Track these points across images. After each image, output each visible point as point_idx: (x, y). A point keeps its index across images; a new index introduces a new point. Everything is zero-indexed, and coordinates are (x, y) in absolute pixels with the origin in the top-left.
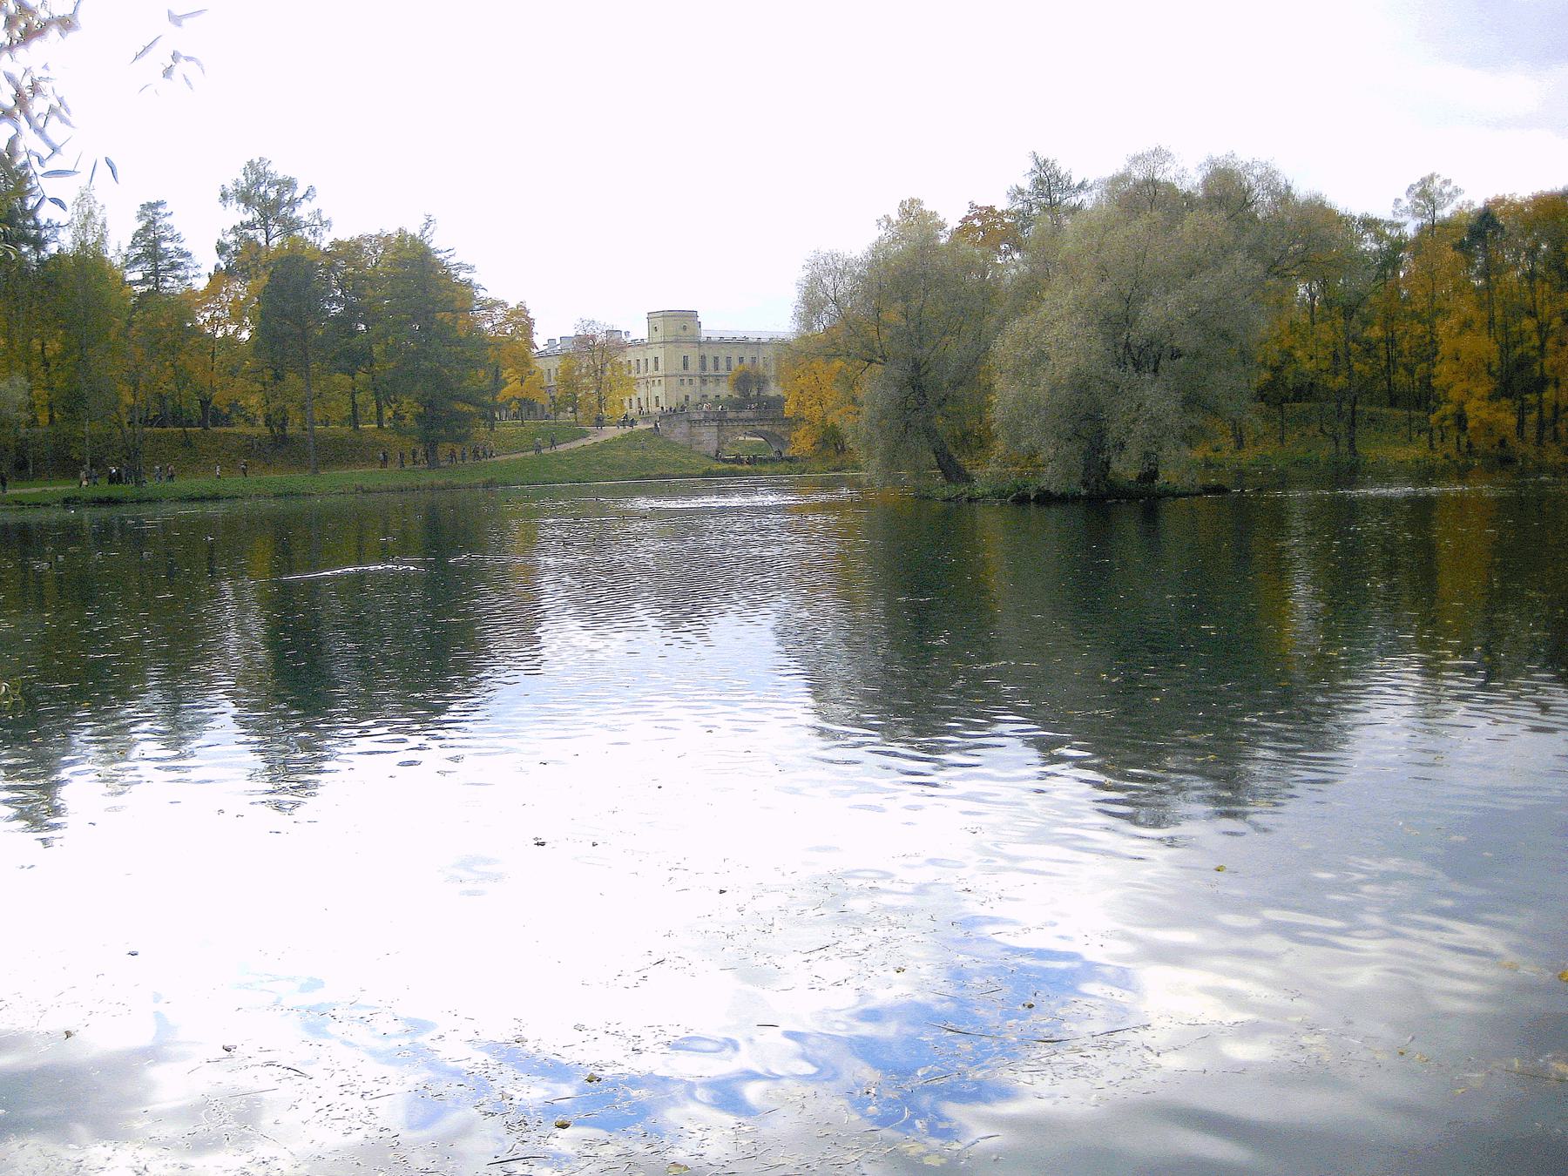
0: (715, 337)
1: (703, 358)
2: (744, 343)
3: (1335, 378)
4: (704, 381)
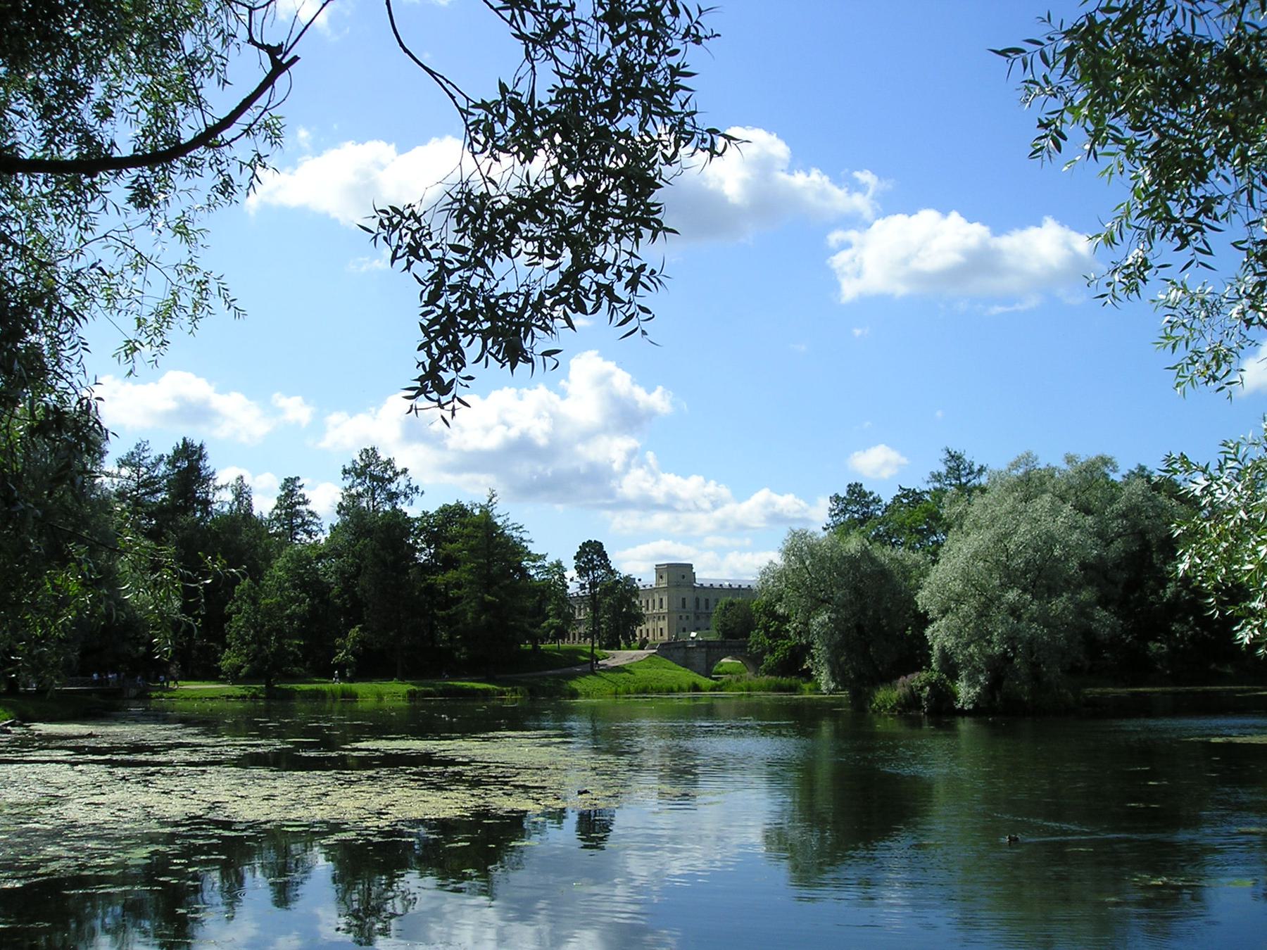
0: (707, 585)
1: (697, 600)
2: (731, 590)
3: (954, 635)
4: (698, 618)
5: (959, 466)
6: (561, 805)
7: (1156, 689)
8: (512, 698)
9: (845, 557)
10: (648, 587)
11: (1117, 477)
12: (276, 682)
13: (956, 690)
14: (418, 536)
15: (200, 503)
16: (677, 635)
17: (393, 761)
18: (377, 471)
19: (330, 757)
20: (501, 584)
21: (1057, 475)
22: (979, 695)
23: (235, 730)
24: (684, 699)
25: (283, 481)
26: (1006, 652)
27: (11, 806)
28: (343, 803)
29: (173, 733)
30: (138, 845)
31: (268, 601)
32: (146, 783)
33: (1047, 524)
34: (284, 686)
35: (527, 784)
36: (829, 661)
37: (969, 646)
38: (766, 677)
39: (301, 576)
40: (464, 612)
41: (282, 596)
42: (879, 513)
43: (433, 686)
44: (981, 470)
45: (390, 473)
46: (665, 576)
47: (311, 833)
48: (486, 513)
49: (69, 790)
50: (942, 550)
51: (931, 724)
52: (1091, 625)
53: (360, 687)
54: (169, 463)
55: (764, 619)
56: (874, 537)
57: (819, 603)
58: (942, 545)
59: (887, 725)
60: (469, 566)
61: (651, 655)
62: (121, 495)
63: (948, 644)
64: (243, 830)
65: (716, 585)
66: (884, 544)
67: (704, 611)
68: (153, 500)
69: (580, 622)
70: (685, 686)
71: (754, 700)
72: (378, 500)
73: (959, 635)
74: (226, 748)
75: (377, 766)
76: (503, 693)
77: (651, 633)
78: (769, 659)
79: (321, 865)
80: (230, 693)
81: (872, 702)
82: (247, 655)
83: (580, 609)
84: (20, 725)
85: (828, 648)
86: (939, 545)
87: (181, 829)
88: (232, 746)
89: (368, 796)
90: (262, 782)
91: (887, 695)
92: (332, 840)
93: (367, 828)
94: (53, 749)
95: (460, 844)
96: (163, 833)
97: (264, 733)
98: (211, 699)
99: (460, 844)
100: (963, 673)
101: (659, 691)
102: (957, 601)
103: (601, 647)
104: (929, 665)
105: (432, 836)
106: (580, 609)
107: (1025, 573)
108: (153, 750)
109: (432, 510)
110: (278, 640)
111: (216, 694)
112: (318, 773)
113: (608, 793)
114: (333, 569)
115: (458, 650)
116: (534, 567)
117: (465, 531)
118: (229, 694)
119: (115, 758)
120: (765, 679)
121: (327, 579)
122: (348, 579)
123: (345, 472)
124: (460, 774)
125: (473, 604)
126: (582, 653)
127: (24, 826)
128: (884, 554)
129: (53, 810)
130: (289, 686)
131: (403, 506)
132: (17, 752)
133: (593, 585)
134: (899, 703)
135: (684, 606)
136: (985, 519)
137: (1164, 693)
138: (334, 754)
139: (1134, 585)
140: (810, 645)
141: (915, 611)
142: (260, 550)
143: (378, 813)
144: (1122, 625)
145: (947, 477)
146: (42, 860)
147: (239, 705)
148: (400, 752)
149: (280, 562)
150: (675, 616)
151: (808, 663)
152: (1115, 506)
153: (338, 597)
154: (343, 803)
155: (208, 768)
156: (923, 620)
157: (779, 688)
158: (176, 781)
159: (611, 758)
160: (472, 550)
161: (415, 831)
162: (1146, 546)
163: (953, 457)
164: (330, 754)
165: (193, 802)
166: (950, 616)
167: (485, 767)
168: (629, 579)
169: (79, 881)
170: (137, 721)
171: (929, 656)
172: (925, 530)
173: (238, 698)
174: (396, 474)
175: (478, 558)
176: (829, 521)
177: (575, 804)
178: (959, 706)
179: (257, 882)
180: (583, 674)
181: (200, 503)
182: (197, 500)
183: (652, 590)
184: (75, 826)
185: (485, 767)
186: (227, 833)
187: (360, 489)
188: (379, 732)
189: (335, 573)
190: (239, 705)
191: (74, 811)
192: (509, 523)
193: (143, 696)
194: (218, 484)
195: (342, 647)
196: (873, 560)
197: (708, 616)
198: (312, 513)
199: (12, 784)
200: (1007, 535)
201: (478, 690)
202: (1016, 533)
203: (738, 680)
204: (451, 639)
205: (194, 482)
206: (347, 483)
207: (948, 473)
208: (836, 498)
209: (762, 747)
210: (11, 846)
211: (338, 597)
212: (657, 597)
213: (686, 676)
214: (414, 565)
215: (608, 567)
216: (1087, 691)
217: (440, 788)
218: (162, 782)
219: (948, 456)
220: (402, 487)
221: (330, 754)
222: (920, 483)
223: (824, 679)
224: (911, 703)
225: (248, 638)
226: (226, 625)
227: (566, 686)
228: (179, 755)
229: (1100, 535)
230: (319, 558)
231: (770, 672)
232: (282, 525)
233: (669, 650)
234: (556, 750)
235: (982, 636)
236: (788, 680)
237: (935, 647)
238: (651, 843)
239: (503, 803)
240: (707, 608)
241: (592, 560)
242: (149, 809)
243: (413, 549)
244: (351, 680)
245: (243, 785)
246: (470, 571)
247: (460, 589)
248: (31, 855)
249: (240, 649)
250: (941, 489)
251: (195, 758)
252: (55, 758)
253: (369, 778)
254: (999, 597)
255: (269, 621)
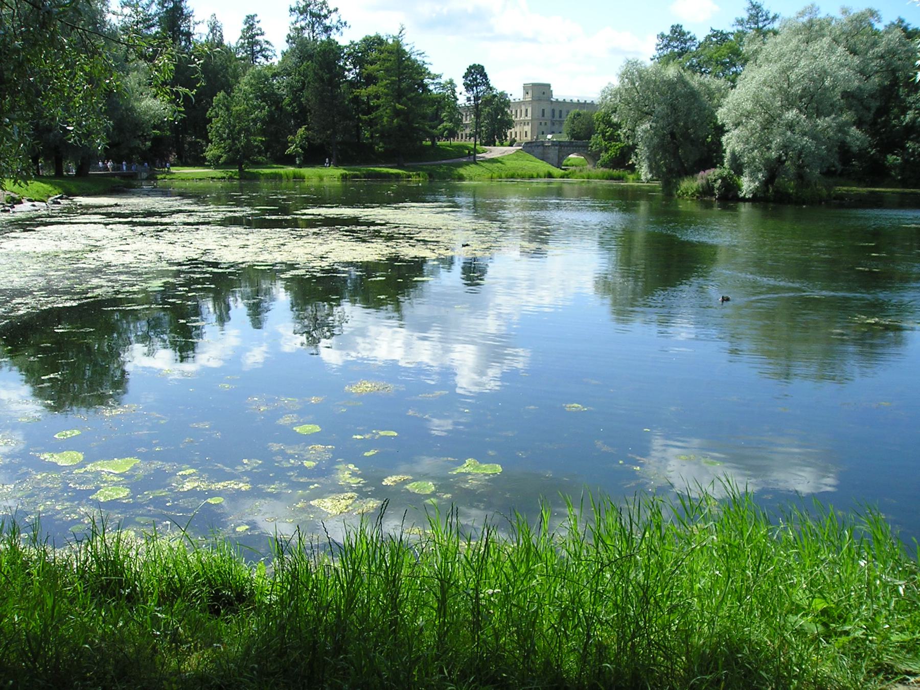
0: (561, 100)
1: (553, 111)
2: (579, 104)
3: (743, 142)
4: (553, 124)
5: (758, 14)
6: (449, 253)
7: (889, 190)
8: (417, 180)
9: (665, 81)
10: (517, 100)
11: (880, 27)
12: (246, 167)
13: (740, 182)
14: (347, 59)
15: (184, 34)
16: (537, 136)
17: (331, 222)
18: (315, 10)
19: (286, 219)
20: (409, 96)
21: (833, 23)
22: (757, 188)
23: (218, 201)
24: (541, 183)
25: (245, 18)
26: (780, 156)
27: (65, 252)
28: (296, 251)
29: (175, 203)
30: (155, 278)
31: (238, 108)
32: (158, 237)
33: (825, 62)
34: (252, 170)
35: (426, 239)
36: (648, 158)
37: (753, 151)
38: (601, 169)
39: (260, 89)
40: (381, 117)
41: (247, 105)
42: (694, 48)
43: (359, 171)
44: (775, 18)
45: (325, 12)
46: (530, 92)
47: (272, 272)
48: (397, 43)
49: (104, 242)
50: (739, 77)
51: (719, 207)
52: (846, 138)
53: (306, 171)
54: (159, 4)
55: (602, 126)
56: (689, 68)
57: (645, 115)
58: (740, 74)
59: (686, 206)
60: (385, 82)
61: (518, 151)
62: (125, 29)
63: (737, 149)
64: (226, 268)
65: (568, 100)
66: (694, 72)
67: (558, 119)
68: (149, 33)
69: (466, 126)
70: (542, 174)
71: (592, 186)
72: (317, 32)
73: (747, 142)
74: (212, 213)
75: (320, 226)
76: (409, 176)
77: (518, 135)
78: (604, 156)
79: (282, 297)
80: (213, 176)
81: (678, 190)
82: (224, 148)
83: (467, 116)
84: (66, 199)
85: (648, 149)
86: (737, 74)
87: (184, 267)
88: (218, 212)
89: (314, 245)
90: (238, 236)
91: (690, 185)
92: (288, 275)
93: (313, 267)
94: (90, 214)
95: (378, 279)
96: (171, 271)
97: (239, 203)
98: (200, 179)
99: (378, 279)
100: (746, 171)
101: (523, 178)
102: (747, 117)
103: (481, 144)
104: (722, 164)
105: (358, 273)
106: (467, 116)
107: (801, 97)
108: (161, 215)
109: (357, 40)
110: (246, 137)
111: (203, 176)
112: (278, 230)
113: (484, 246)
114: (284, 84)
115: (377, 144)
116: (433, 83)
117: (382, 56)
118: (213, 176)
119: (135, 220)
120: (601, 171)
121: (280, 92)
122: (296, 92)
123: (291, 10)
124: (379, 232)
125: (388, 111)
126: (467, 148)
127: (75, 266)
128: (695, 80)
129: (94, 255)
130: (255, 170)
131: (335, 36)
132: (66, 216)
133: (477, 98)
134: (697, 191)
135: (543, 116)
136: (774, 55)
137: (893, 193)
138: (289, 217)
139: (883, 111)
140: (635, 146)
141: (715, 124)
142: (230, 70)
143: (321, 257)
144: (869, 141)
145: (748, 22)
146: (90, 288)
147: (220, 184)
148: (336, 216)
149: (245, 80)
150: (537, 123)
151: (633, 160)
152: (876, 49)
153: (289, 105)
154: (296, 251)
155: (200, 227)
156: (721, 130)
157: (611, 178)
158: (178, 235)
159: (487, 223)
160: (387, 70)
161: (347, 269)
162: (895, 82)
163: (754, 6)
164: (286, 217)
165: (191, 249)
166: (741, 128)
167: (396, 227)
168: (503, 95)
169: (114, 302)
170: (148, 195)
171: (723, 157)
172: (728, 63)
173: (219, 179)
174: (330, 12)
175: (391, 76)
176: (656, 54)
177: (461, 255)
178: (742, 195)
179: (239, 308)
180: (467, 164)
181: (184, 34)
182: (182, 33)
183: (520, 103)
184: (110, 266)
185: (396, 227)
186: (216, 270)
187: (303, 24)
188: (319, 202)
189: (286, 87)
190: (220, 184)
191: (108, 256)
192: (414, 50)
193: (152, 178)
194: (196, 19)
195: (293, 142)
196: (685, 84)
197: (561, 123)
198: (267, 42)
199: (65, 238)
200: (791, 68)
201: (392, 174)
202: (797, 66)
203: (581, 171)
204: (372, 137)
205: (179, 19)
206: (294, 18)
207: (749, 19)
208: (662, 36)
209: (595, 218)
210: (68, 279)
211: (289, 105)
212: (523, 108)
213: (544, 167)
214: (345, 82)
215: (487, 84)
216: (837, 188)
217: (364, 241)
218: (168, 236)
219: (750, 5)
220: (334, 23)
221: (286, 217)
222: (728, 26)
223: (644, 172)
224: (707, 190)
225: (225, 136)
226: (208, 126)
227: (456, 172)
228: (181, 218)
229: (862, 72)
230: (274, 76)
231: (604, 165)
232: (246, 52)
233: (531, 147)
234: (447, 216)
235: (764, 144)
236: (617, 172)
237: (728, 151)
238: (511, 284)
239: (409, 252)
240: (560, 117)
241: (476, 79)
242: (160, 254)
243: (343, 69)
244: (300, 166)
245: (226, 238)
246: (386, 86)
247: (378, 99)
248: (82, 284)
249: (219, 143)
250: (743, 31)
251: (191, 220)
252: (93, 221)
253: (314, 233)
254: (780, 116)
255: (239, 123)
